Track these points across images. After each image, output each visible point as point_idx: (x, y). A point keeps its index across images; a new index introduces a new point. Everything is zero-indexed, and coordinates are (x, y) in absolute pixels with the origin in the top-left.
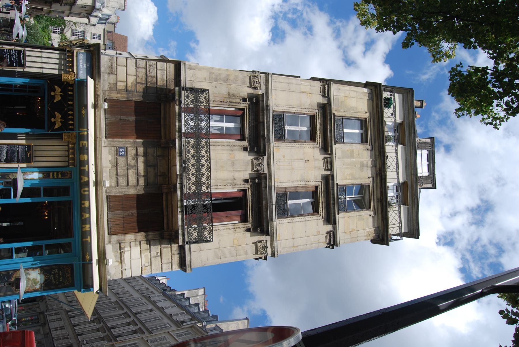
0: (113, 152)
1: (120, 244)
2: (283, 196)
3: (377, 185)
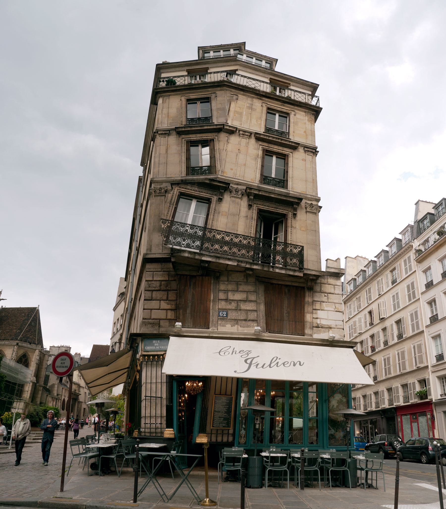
0: (223, 322)
1: (313, 327)
2: (265, 179)
3: (269, 102)
